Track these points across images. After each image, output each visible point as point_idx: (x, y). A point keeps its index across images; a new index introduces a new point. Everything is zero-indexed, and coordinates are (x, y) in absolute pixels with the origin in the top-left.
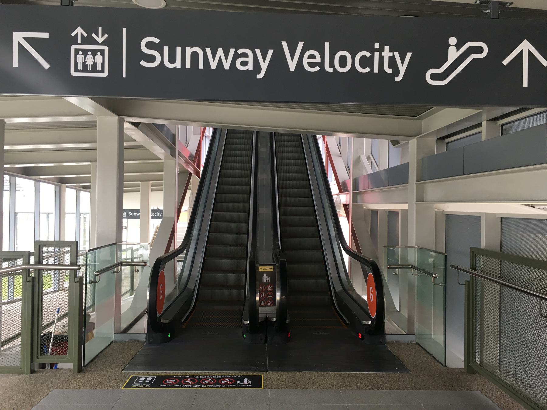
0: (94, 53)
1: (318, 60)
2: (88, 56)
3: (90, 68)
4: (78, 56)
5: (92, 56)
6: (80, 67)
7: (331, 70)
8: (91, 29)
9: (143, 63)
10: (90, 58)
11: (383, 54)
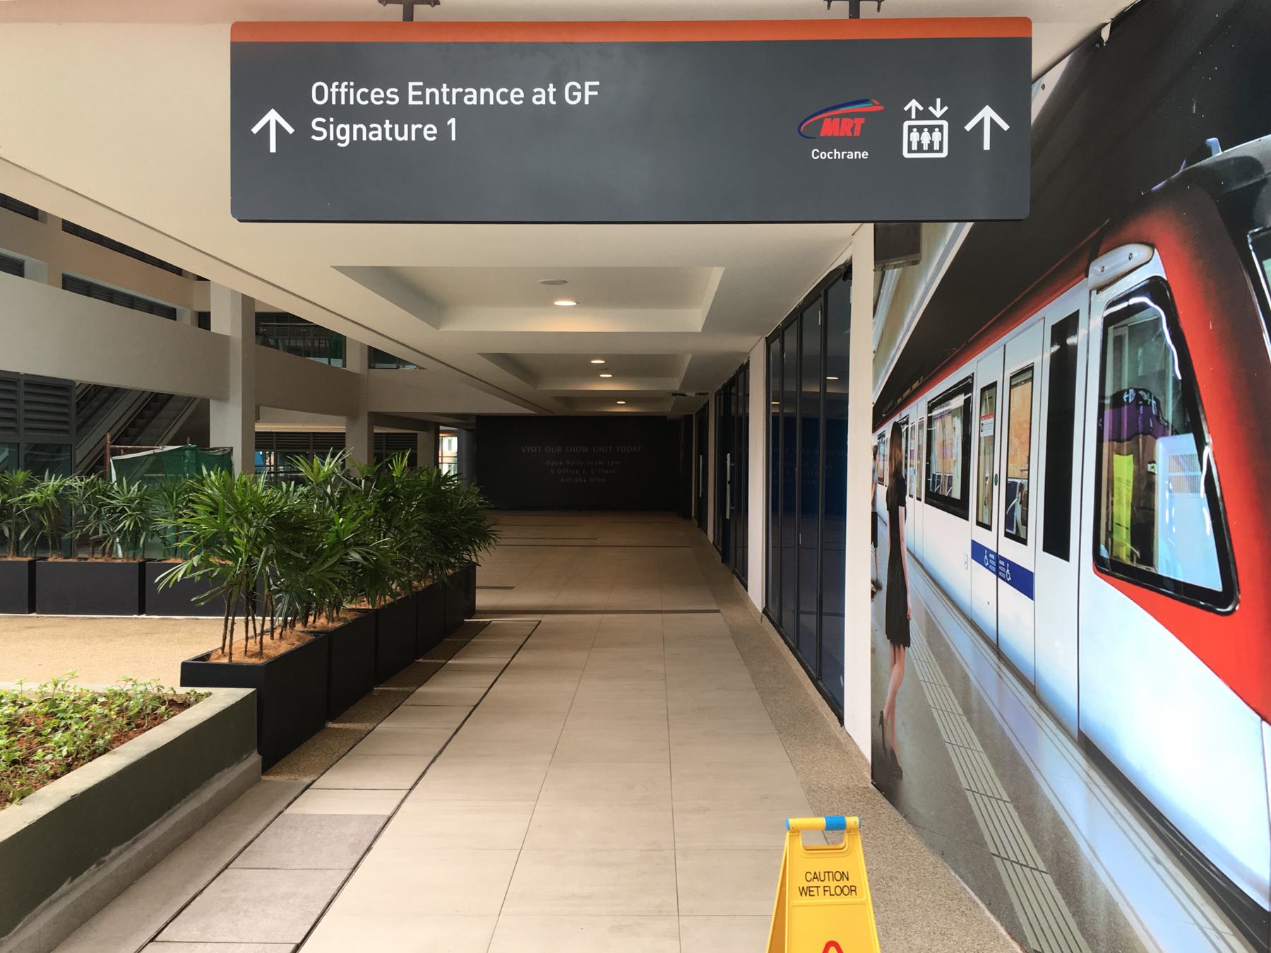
0: (931, 129)
2: (923, 133)
3: (926, 148)
4: (912, 134)
5: (928, 133)
6: (915, 147)
7: (390, 139)
8: (927, 101)
9: (314, 137)
10: (926, 135)
11: (549, 90)
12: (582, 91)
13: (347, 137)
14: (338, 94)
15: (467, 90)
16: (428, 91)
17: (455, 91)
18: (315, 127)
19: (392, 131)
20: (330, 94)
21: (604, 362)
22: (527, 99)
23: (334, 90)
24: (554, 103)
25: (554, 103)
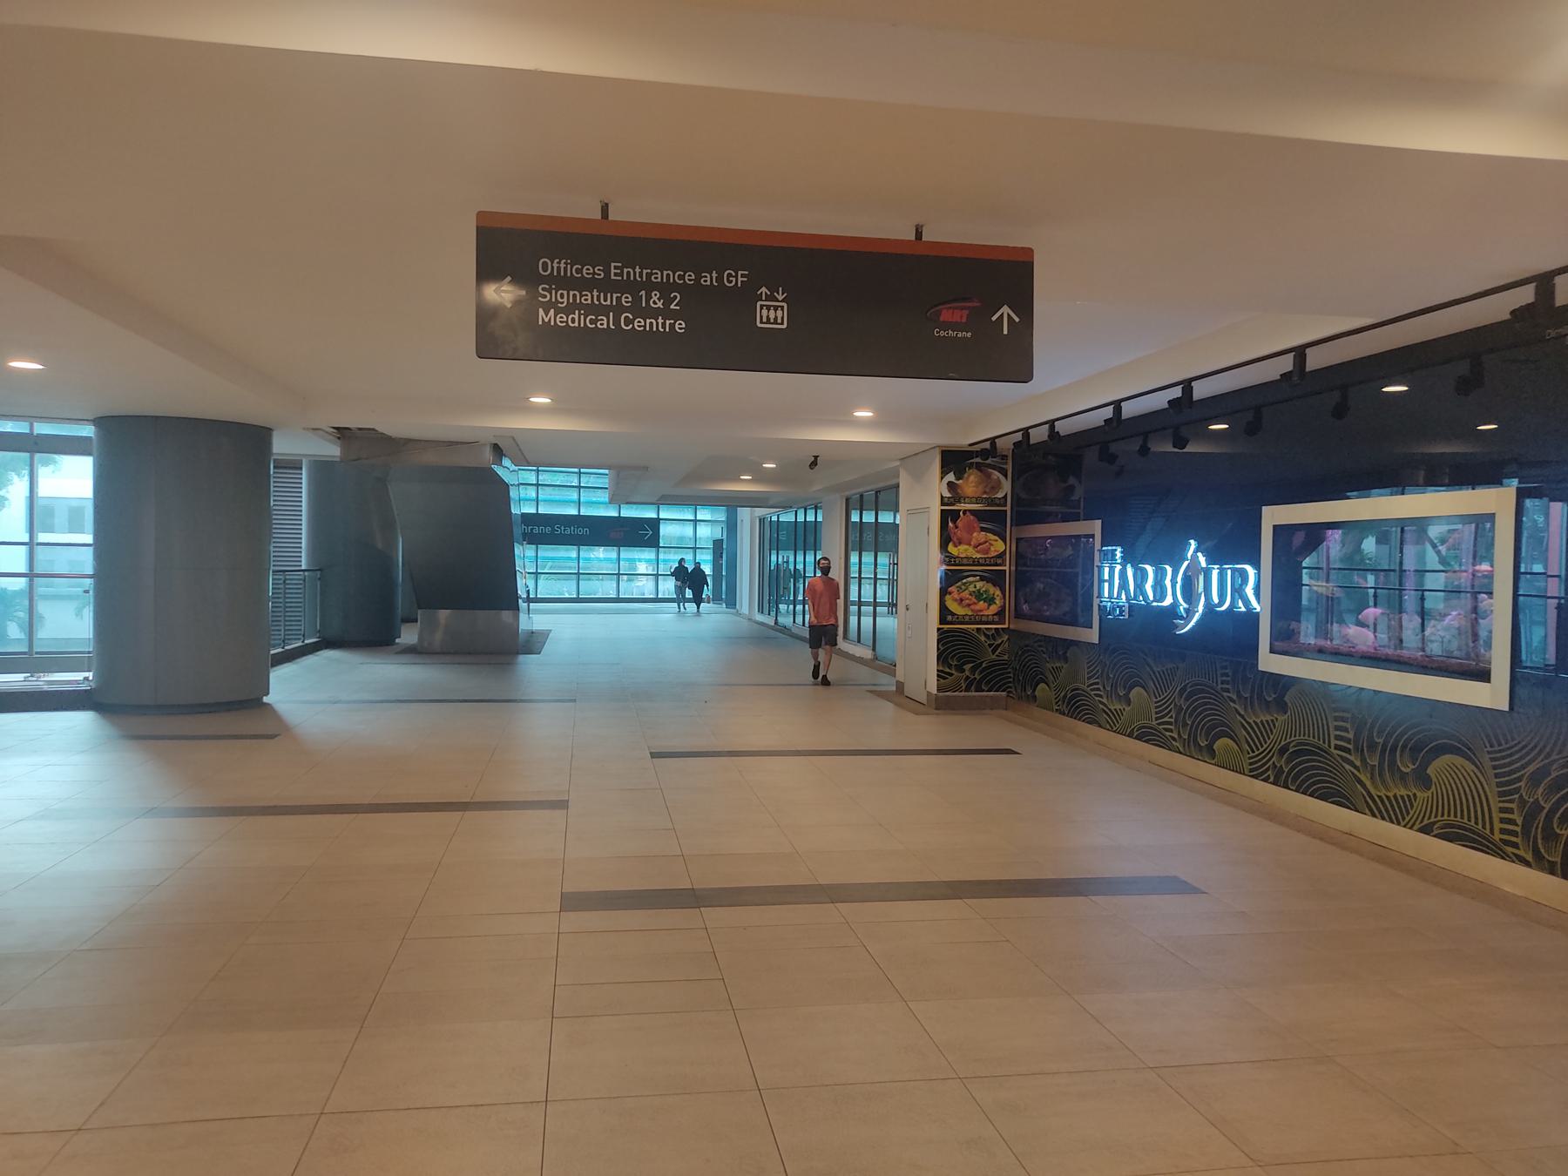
0: (776, 308)
1: (693, 277)
3: (772, 321)
6: (765, 320)
7: (597, 303)
8: (773, 289)
12: (736, 277)
13: (565, 300)
14: (559, 268)
15: (654, 271)
16: (625, 270)
17: (645, 271)
18: (541, 291)
19: (599, 297)
20: (552, 267)
21: (1227, 426)
22: (697, 280)
23: (555, 265)
24: (716, 284)
25: (716, 284)
